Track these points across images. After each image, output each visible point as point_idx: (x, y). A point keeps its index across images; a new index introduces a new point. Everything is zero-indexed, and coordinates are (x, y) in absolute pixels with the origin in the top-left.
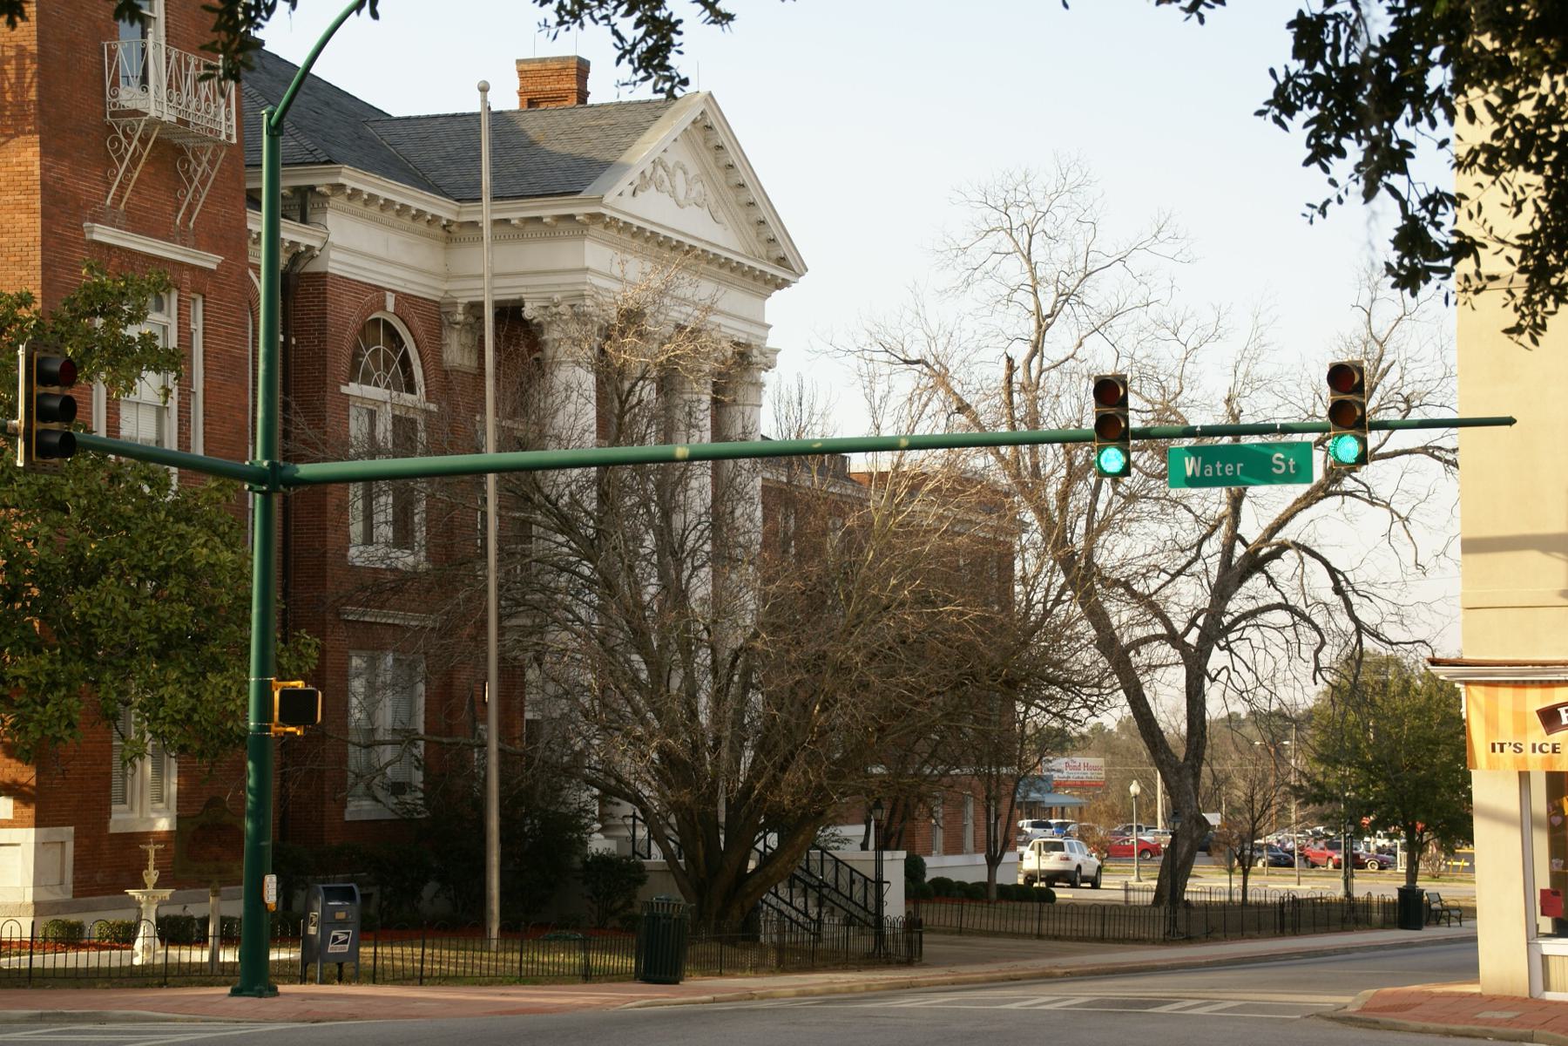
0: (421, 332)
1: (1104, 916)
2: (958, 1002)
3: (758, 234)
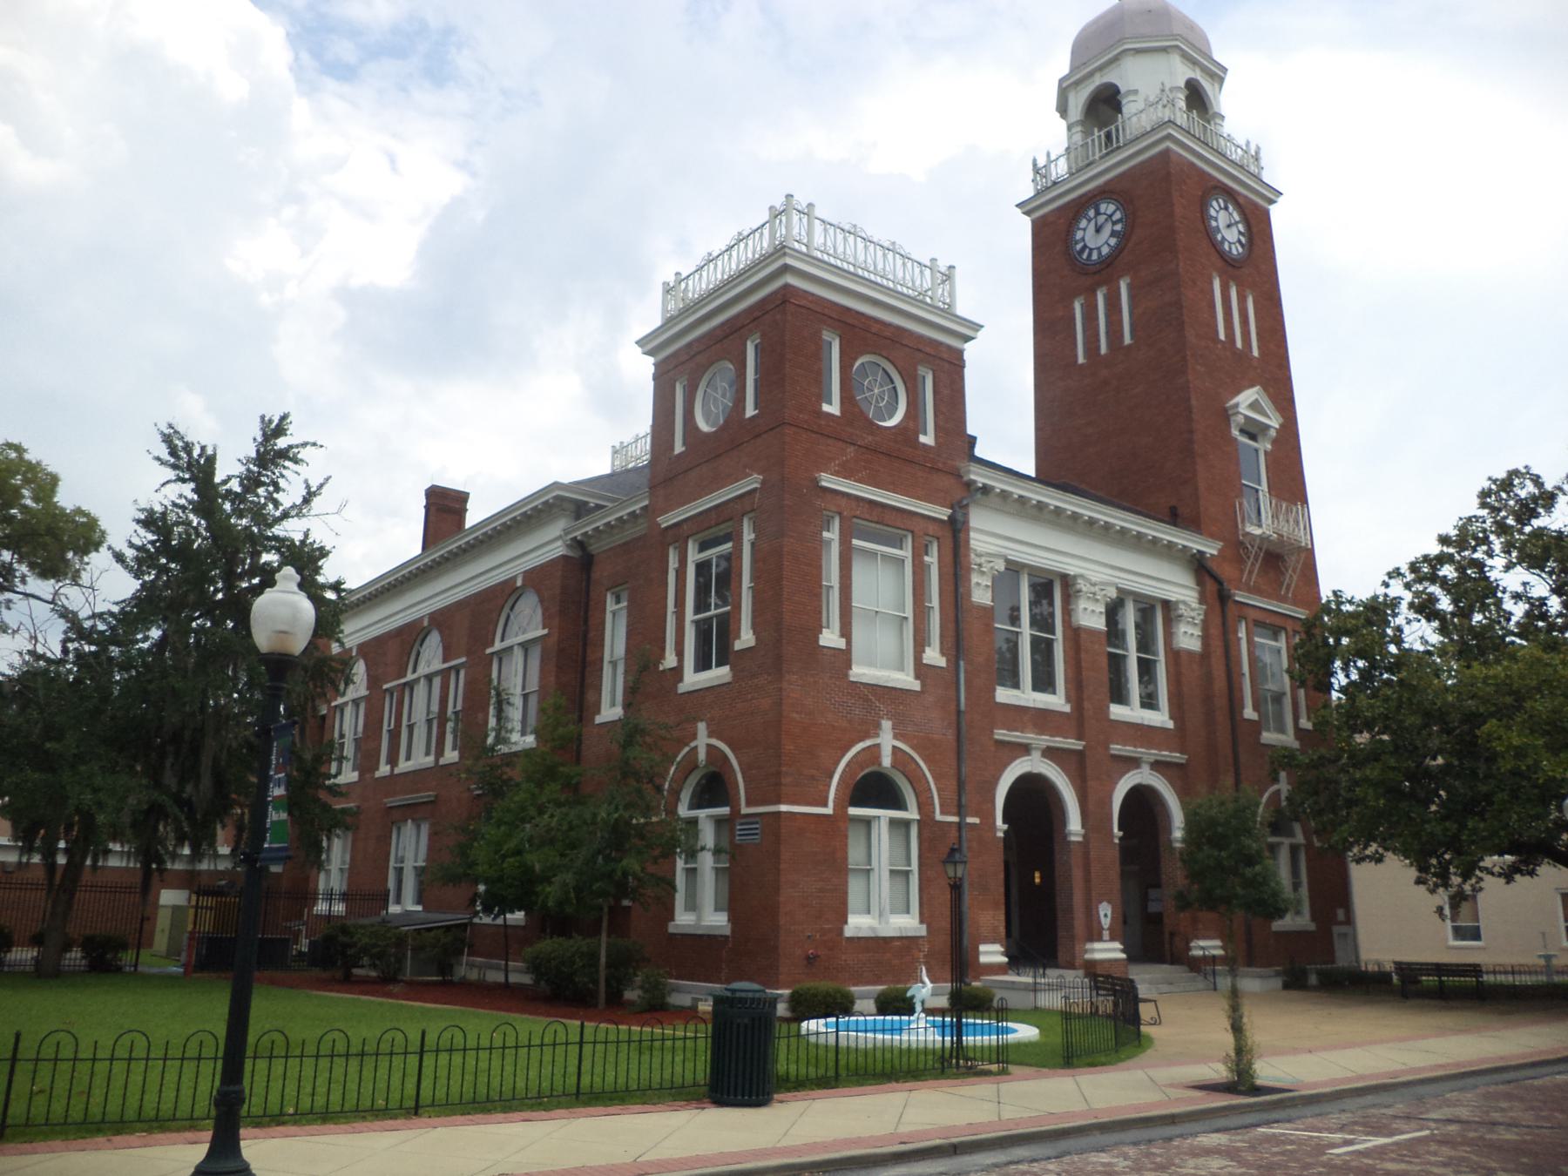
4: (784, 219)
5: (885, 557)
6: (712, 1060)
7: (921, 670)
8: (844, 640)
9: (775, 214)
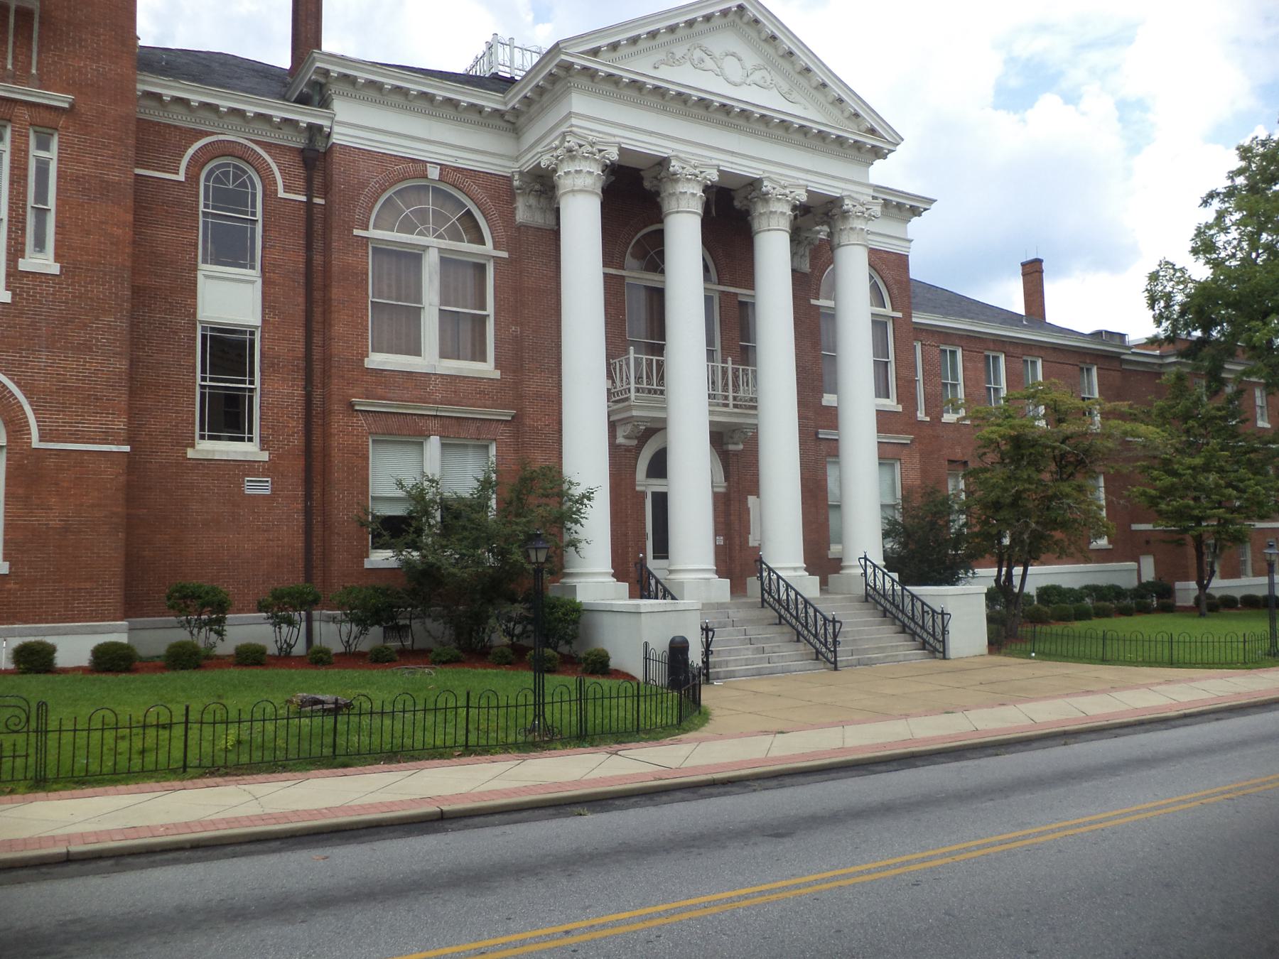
3: (843, 112)
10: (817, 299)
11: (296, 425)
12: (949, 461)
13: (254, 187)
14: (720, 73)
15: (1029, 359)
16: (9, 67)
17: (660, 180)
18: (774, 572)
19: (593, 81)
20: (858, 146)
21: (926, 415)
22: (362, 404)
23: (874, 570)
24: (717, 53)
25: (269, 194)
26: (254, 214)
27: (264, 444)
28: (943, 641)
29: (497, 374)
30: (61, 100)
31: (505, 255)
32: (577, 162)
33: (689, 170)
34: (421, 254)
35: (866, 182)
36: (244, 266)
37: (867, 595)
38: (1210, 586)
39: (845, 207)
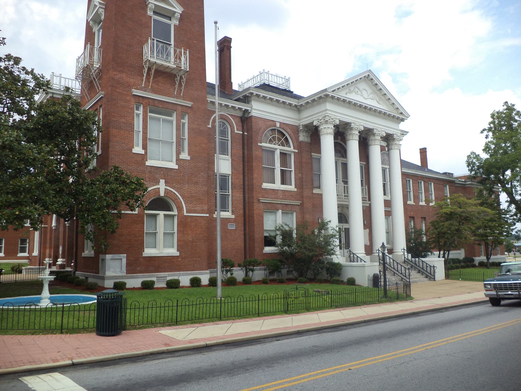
0: (293, 137)
1: (62, 329)
2: (359, 364)
3: (393, 107)
4: (263, 75)
5: (164, 120)
6: (97, 316)
7: (179, 161)
8: (144, 151)
9: (261, 73)
10: (261, 143)
11: (241, 206)
12: (410, 217)
13: (228, 129)
14: (362, 95)
15: (430, 183)
16: (175, 93)
17: (346, 129)
18: (355, 255)
19: (333, 99)
20: (398, 118)
21: (414, 203)
22: (263, 200)
23: (354, 255)
24: (361, 89)
25: (232, 131)
26: (228, 138)
27: (233, 213)
28: (434, 275)
29: (296, 190)
30: (189, 104)
31: (297, 151)
32: (328, 124)
33: (356, 126)
34: (274, 151)
35: (397, 129)
36: (225, 155)
37: (405, 261)
38: (491, 258)
39: (352, 126)
